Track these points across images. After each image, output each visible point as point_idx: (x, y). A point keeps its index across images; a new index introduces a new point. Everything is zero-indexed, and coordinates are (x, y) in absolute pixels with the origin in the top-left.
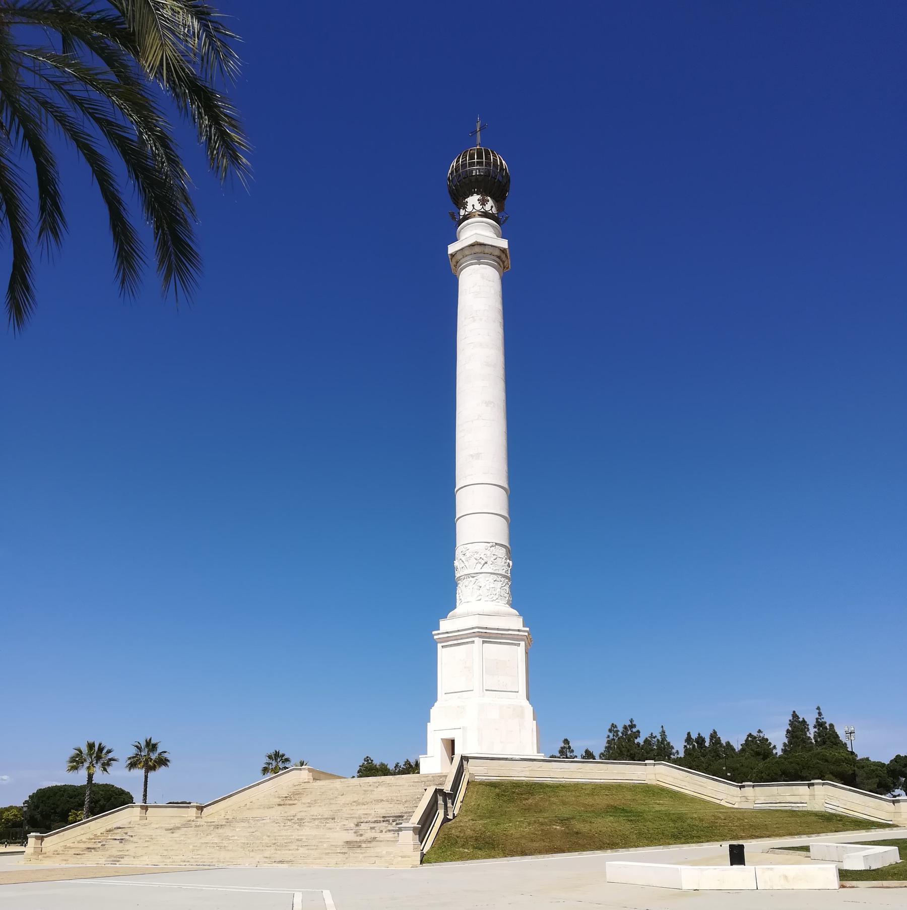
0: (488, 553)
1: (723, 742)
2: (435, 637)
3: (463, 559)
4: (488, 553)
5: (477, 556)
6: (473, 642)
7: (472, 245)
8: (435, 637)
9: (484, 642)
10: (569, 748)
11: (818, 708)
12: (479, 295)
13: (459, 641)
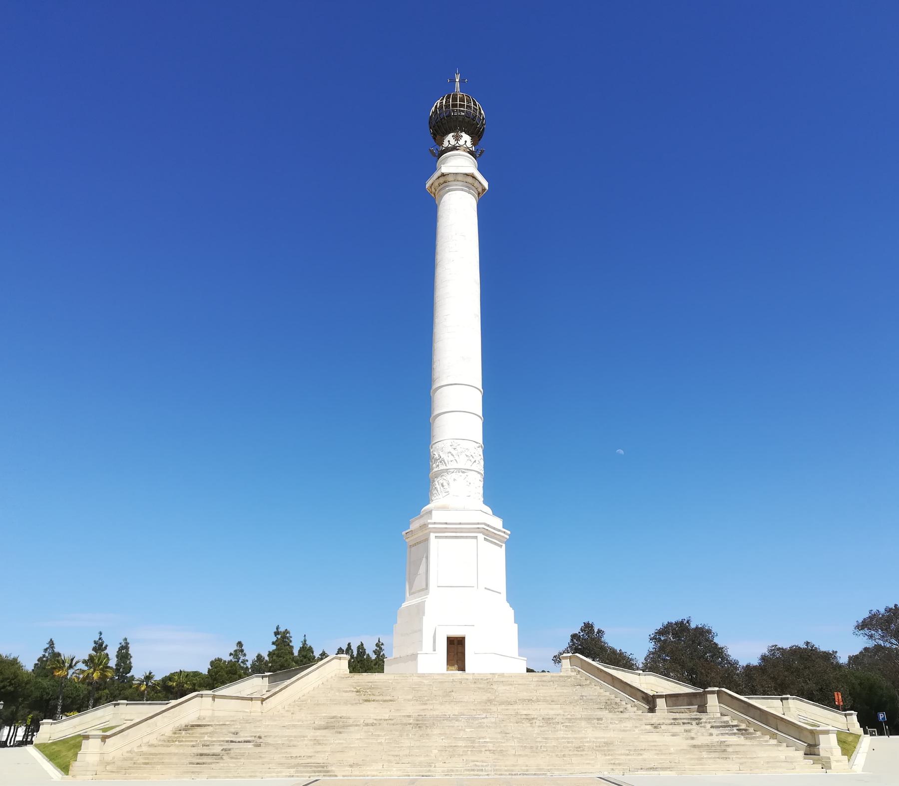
1: (274, 647)
2: (430, 526)
7: (467, 175)
8: (430, 526)
10: (242, 651)
11: (101, 633)
12: (459, 220)
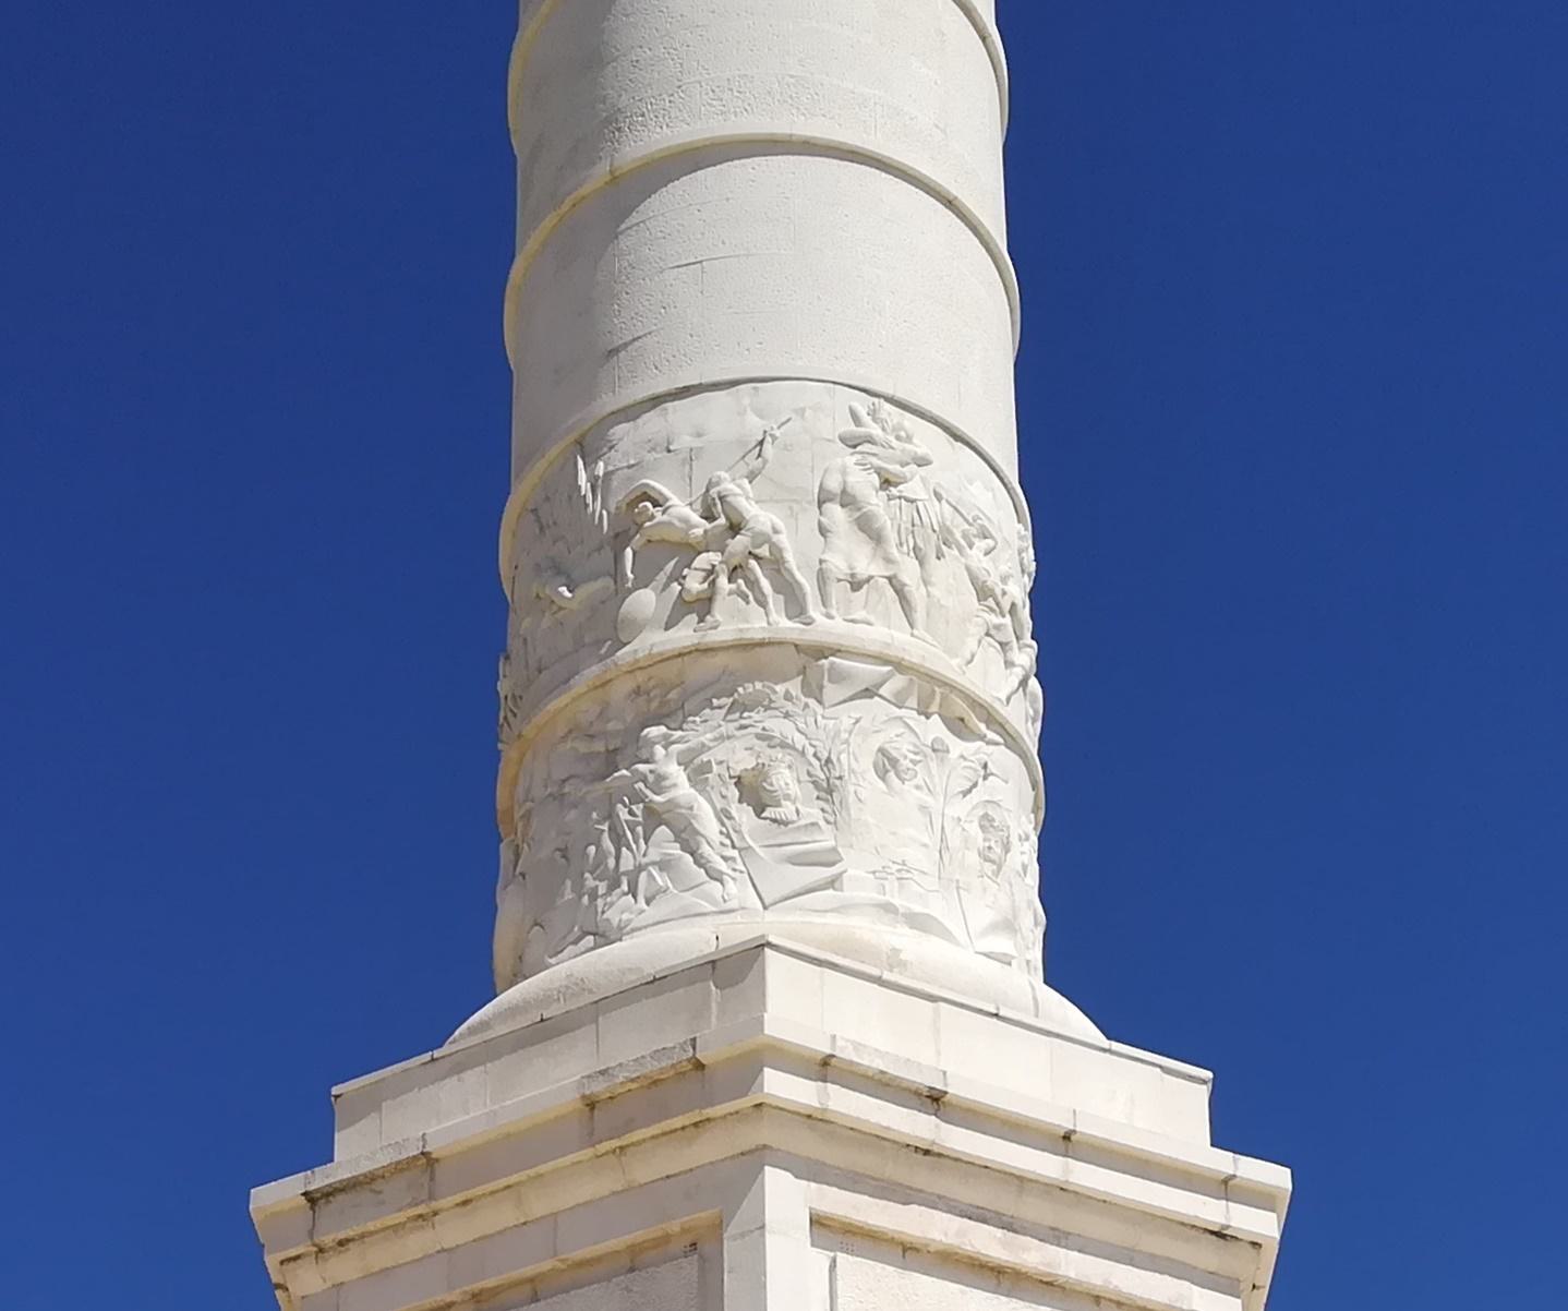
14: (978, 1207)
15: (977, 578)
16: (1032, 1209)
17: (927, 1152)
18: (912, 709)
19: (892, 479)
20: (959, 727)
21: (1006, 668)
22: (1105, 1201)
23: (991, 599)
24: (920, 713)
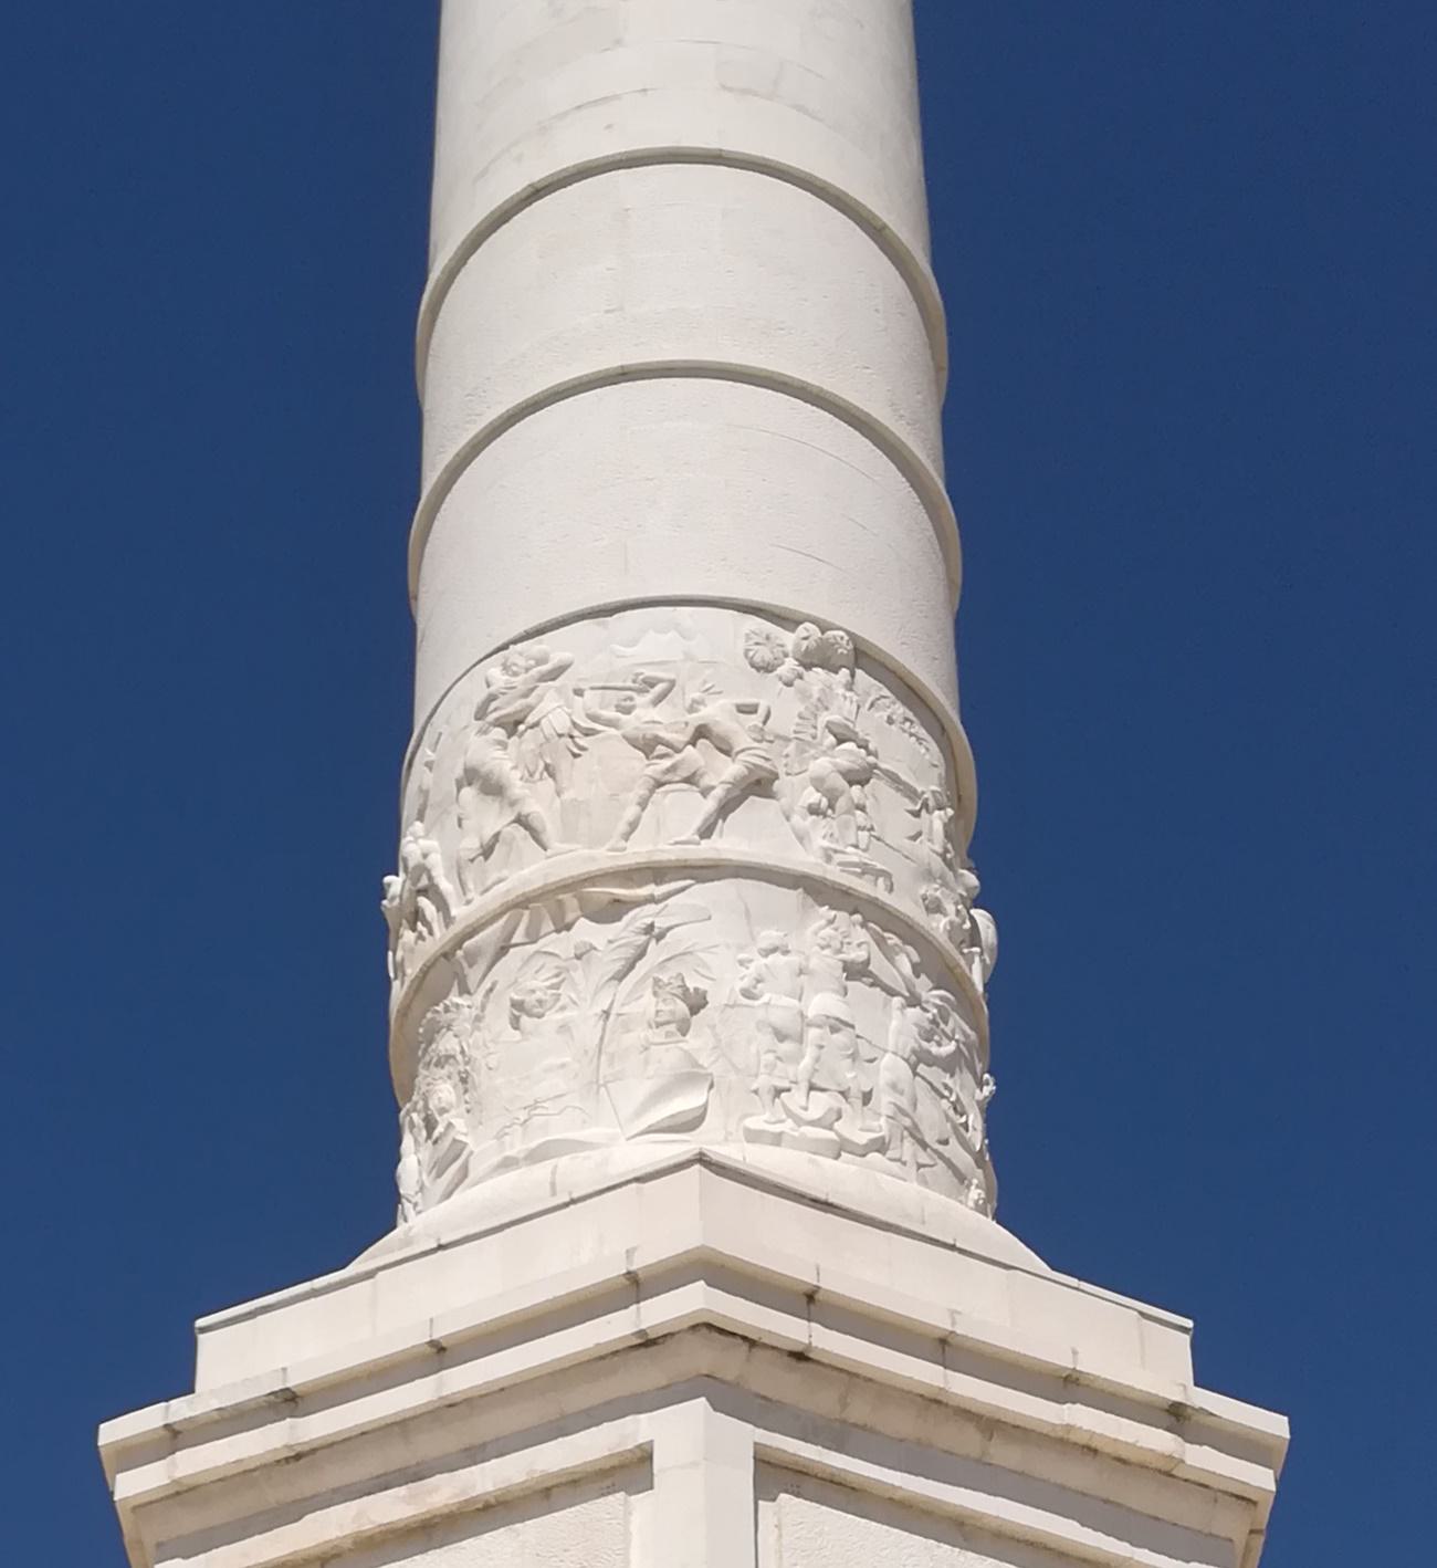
0: (786, 710)
3: (502, 760)
4: (786, 710)
5: (666, 719)
6: (633, 1471)
8: (129, 1486)
9: (773, 1476)
13: (443, 1492)
14: (378, 1477)
15: (637, 739)
16: (429, 1445)
17: (298, 1457)
18: (549, 933)
19: (517, 717)
20: (612, 911)
21: (705, 797)
22: (502, 1389)
23: (660, 747)
24: (558, 931)
